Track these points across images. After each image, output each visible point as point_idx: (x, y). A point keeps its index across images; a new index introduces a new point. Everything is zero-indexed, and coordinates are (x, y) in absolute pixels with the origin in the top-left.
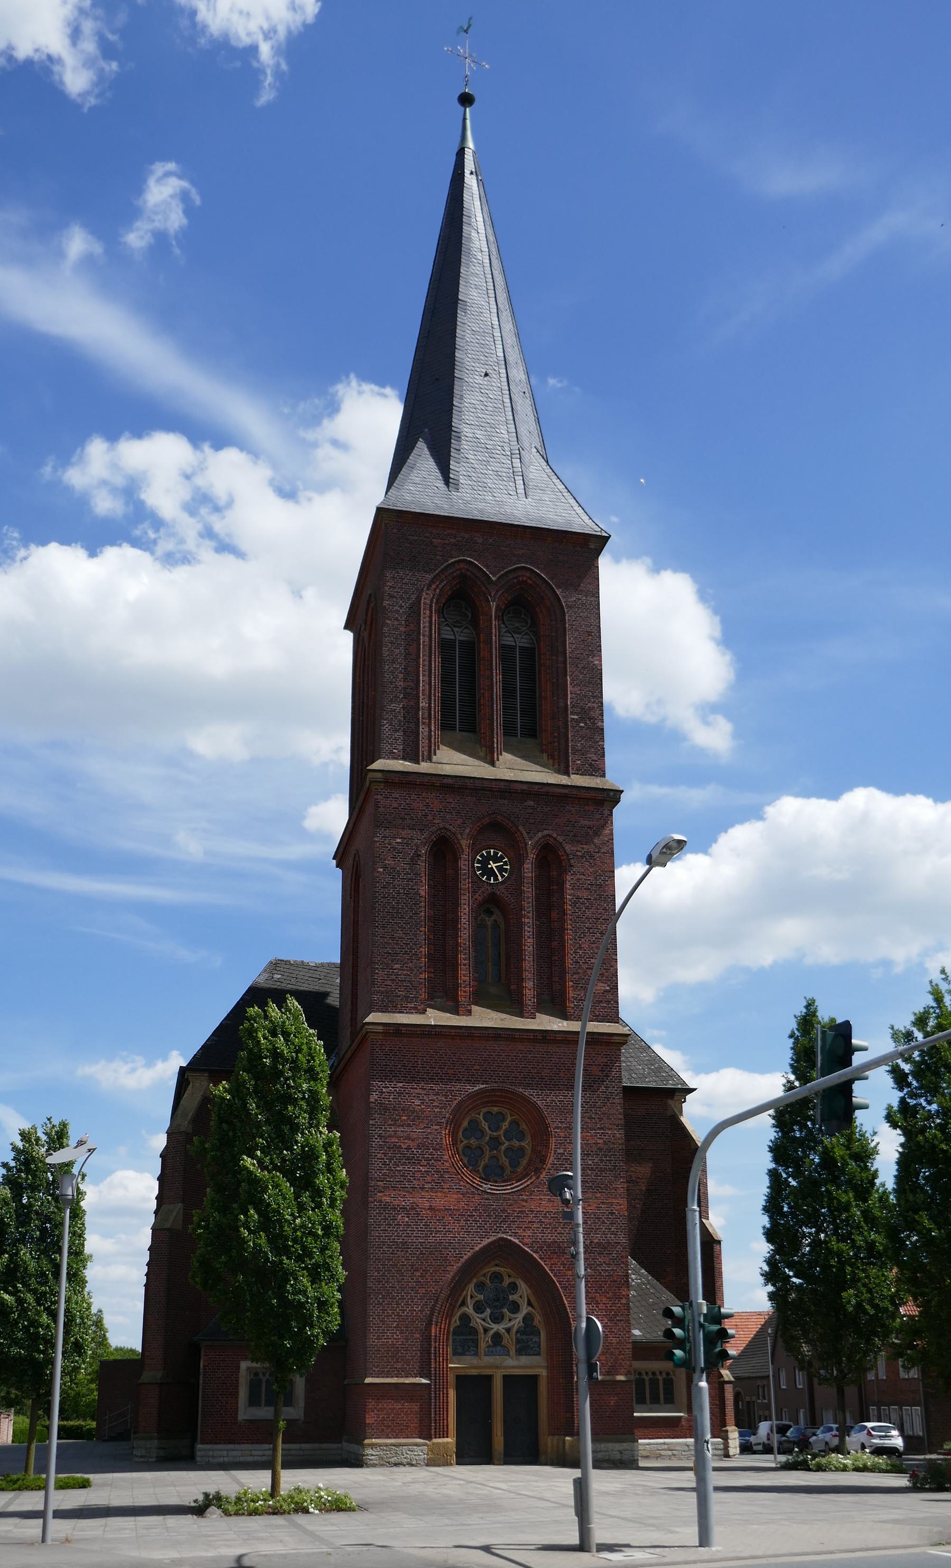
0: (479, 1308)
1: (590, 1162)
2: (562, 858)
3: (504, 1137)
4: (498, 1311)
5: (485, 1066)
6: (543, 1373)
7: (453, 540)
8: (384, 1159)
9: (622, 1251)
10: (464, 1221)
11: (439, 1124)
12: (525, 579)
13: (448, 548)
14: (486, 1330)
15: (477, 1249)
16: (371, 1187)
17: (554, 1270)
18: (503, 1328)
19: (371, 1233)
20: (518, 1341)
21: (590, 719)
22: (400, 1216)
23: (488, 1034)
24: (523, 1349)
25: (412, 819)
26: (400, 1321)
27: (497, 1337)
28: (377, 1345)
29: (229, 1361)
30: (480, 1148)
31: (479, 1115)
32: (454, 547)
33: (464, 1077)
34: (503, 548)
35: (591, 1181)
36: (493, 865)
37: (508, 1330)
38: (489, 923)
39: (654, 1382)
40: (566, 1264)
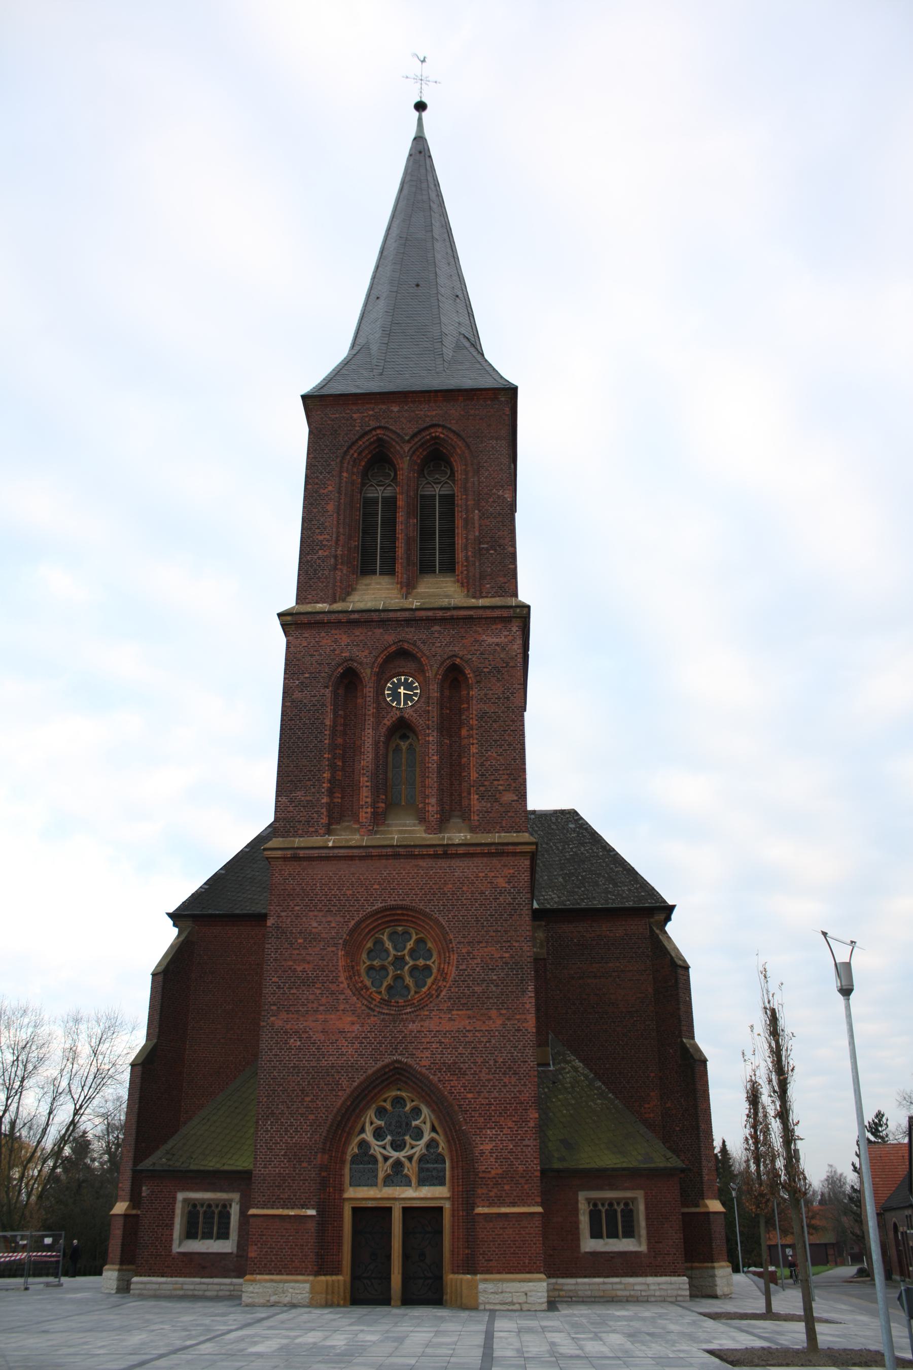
0: (378, 1134)
1: (495, 978)
2: (468, 676)
3: (399, 951)
4: (401, 1138)
5: (385, 885)
6: (447, 1205)
7: (371, 413)
8: (278, 983)
9: (529, 1071)
10: (358, 1043)
11: (335, 945)
12: (437, 434)
13: (367, 419)
14: (386, 1159)
15: (370, 1072)
16: (264, 1010)
17: (453, 1093)
18: (404, 1157)
19: (262, 1058)
20: (421, 1170)
21: (500, 546)
22: (292, 1040)
23: (387, 852)
24: (428, 1177)
25: (321, 655)
26: (287, 1149)
27: (398, 1164)
28: (263, 1174)
29: (167, 1192)
30: (383, 968)
31: (383, 935)
32: (372, 418)
33: (362, 897)
34: (417, 412)
35: (496, 998)
36: (402, 690)
37: (410, 1158)
38: (404, 748)
39: (209, 1215)
40: (467, 1086)
